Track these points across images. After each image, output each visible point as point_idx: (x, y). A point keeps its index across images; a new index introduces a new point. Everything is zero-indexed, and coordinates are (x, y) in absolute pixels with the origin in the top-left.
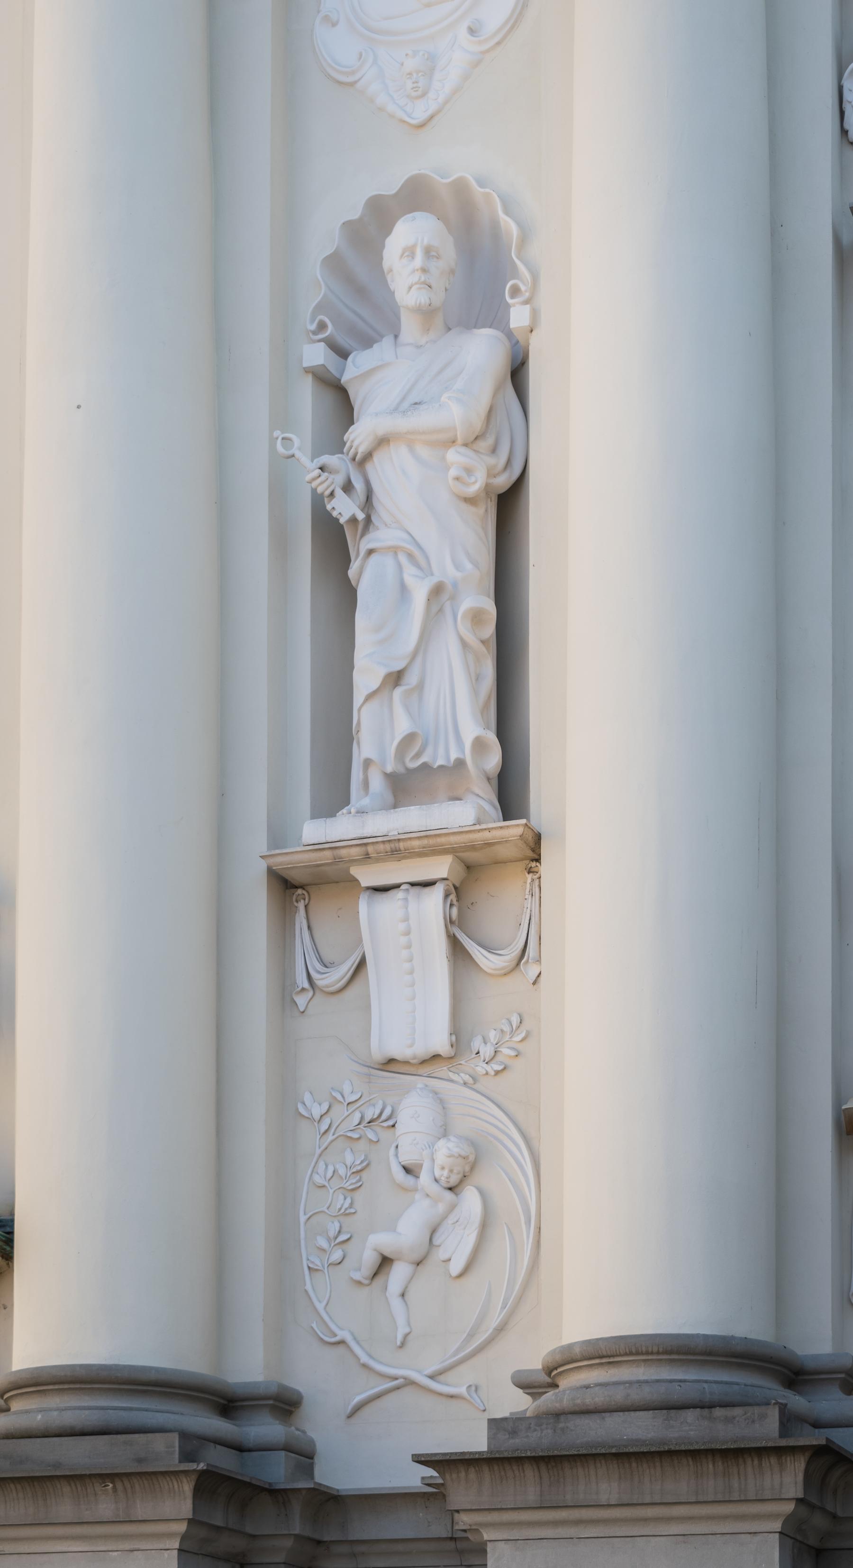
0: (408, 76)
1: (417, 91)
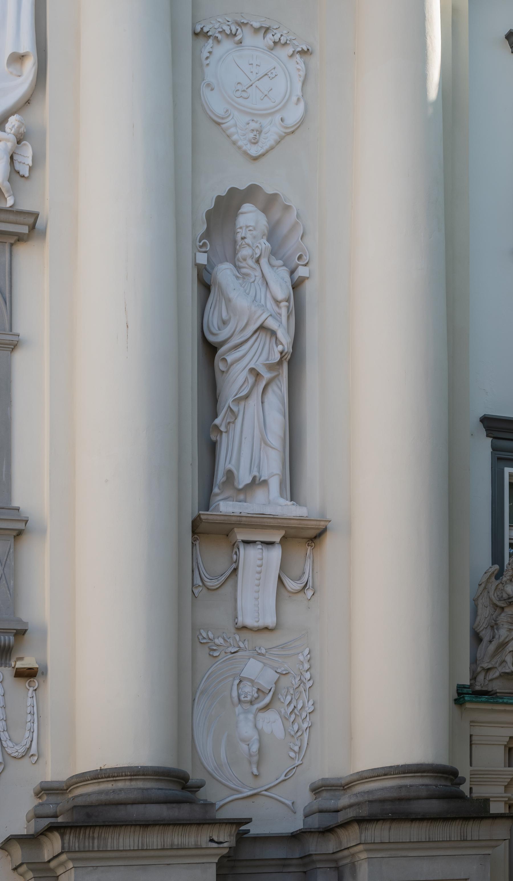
0: (252, 131)
1: (255, 140)
